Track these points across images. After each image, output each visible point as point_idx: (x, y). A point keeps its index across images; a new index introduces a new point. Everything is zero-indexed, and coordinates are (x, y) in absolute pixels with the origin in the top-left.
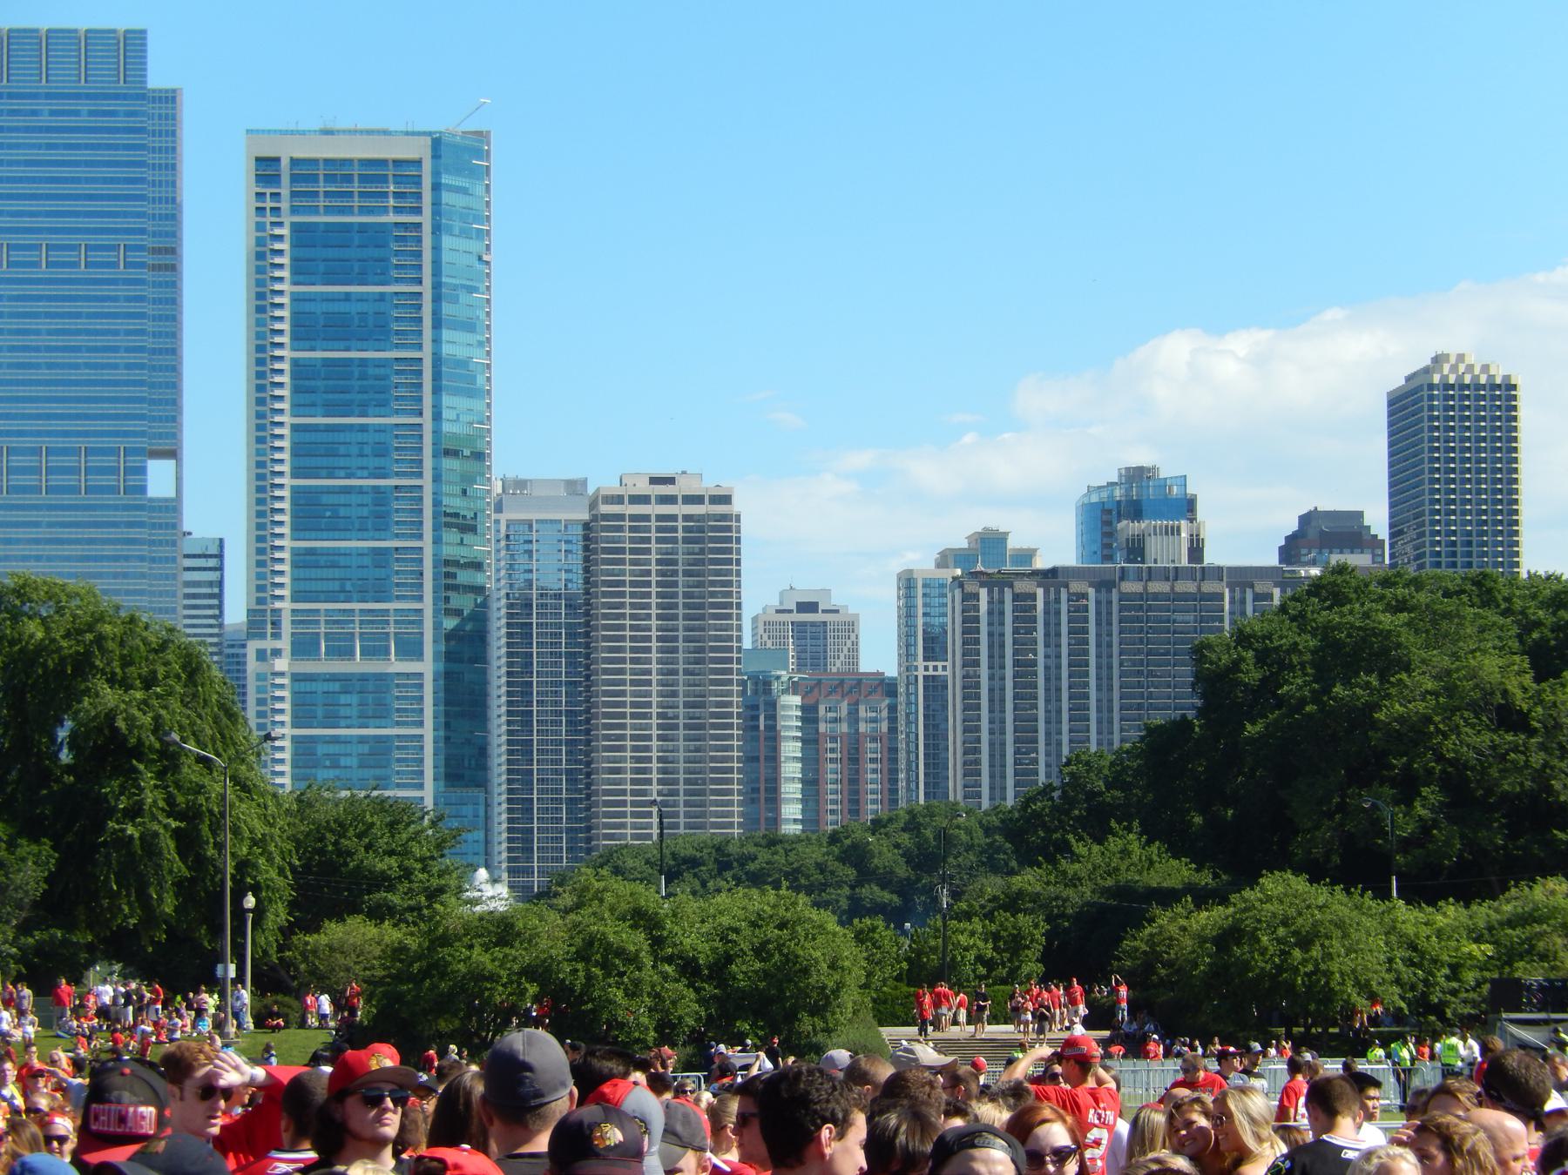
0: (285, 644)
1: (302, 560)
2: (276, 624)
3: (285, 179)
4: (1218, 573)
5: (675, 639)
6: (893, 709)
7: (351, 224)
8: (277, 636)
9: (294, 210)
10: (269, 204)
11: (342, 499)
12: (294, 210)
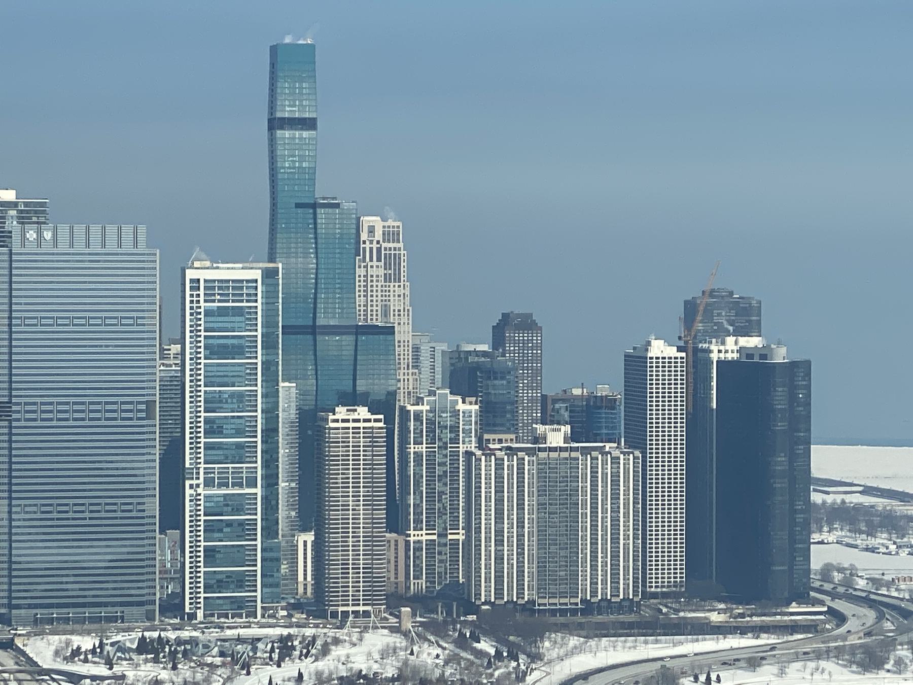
0: (201, 480)
1: (208, 447)
2: (198, 473)
5: (359, 487)
6: (644, 586)
7: (229, 307)
8: (198, 478)
9: (205, 301)
10: (195, 299)
11: (225, 421)
12: (205, 301)
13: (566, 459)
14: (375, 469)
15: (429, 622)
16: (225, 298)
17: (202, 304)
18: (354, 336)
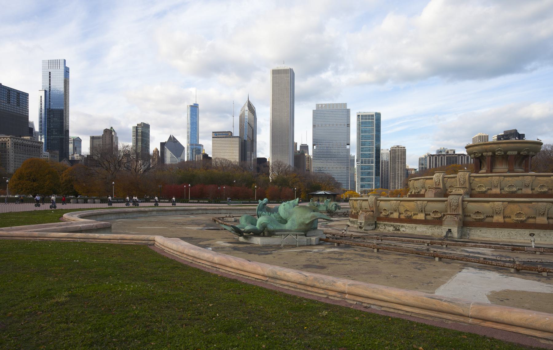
0: (360, 162)
2: (359, 160)
3: (360, 117)
4: (457, 154)
8: (359, 162)
13: (454, 157)
14: (346, 160)
15: (316, 191)
16: (366, 119)
17: (360, 121)
18: (238, 135)
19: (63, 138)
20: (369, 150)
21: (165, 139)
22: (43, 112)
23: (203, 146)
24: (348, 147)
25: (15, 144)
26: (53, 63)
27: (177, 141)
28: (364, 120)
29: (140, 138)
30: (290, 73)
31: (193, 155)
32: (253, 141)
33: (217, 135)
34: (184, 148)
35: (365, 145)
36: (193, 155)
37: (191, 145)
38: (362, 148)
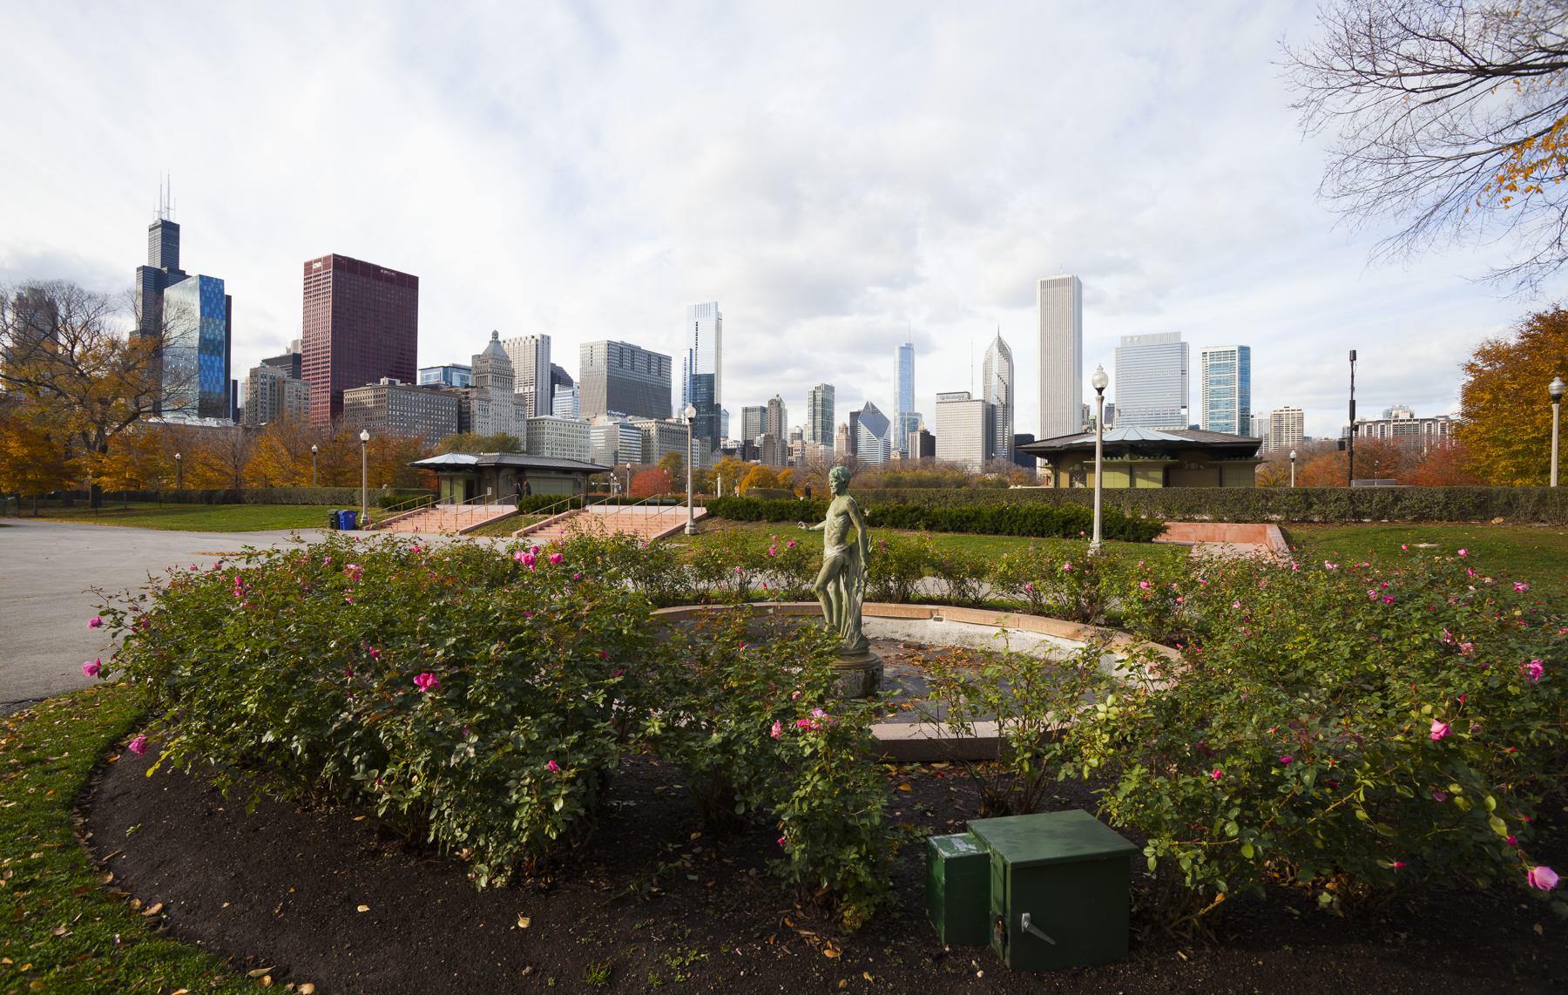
4: (1417, 420)
16: (1219, 359)
18: (982, 398)
19: (713, 417)
20: (1227, 417)
21: (859, 407)
22: (688, 380)
23: (921, 415)
24: (1184, 412)
25: (661, 430)
26: (702, 309)
27: (878, 411)
28: (1215, 360)
29: (819, 408)
30: (1075, 285)
31: (904, 433)
32: (1008, 406)
33: (944, 398)
34: (887, 422)
35: (1217, 408)
36: (904, 433)
37: (902, 414)
38: (1211, 413)
